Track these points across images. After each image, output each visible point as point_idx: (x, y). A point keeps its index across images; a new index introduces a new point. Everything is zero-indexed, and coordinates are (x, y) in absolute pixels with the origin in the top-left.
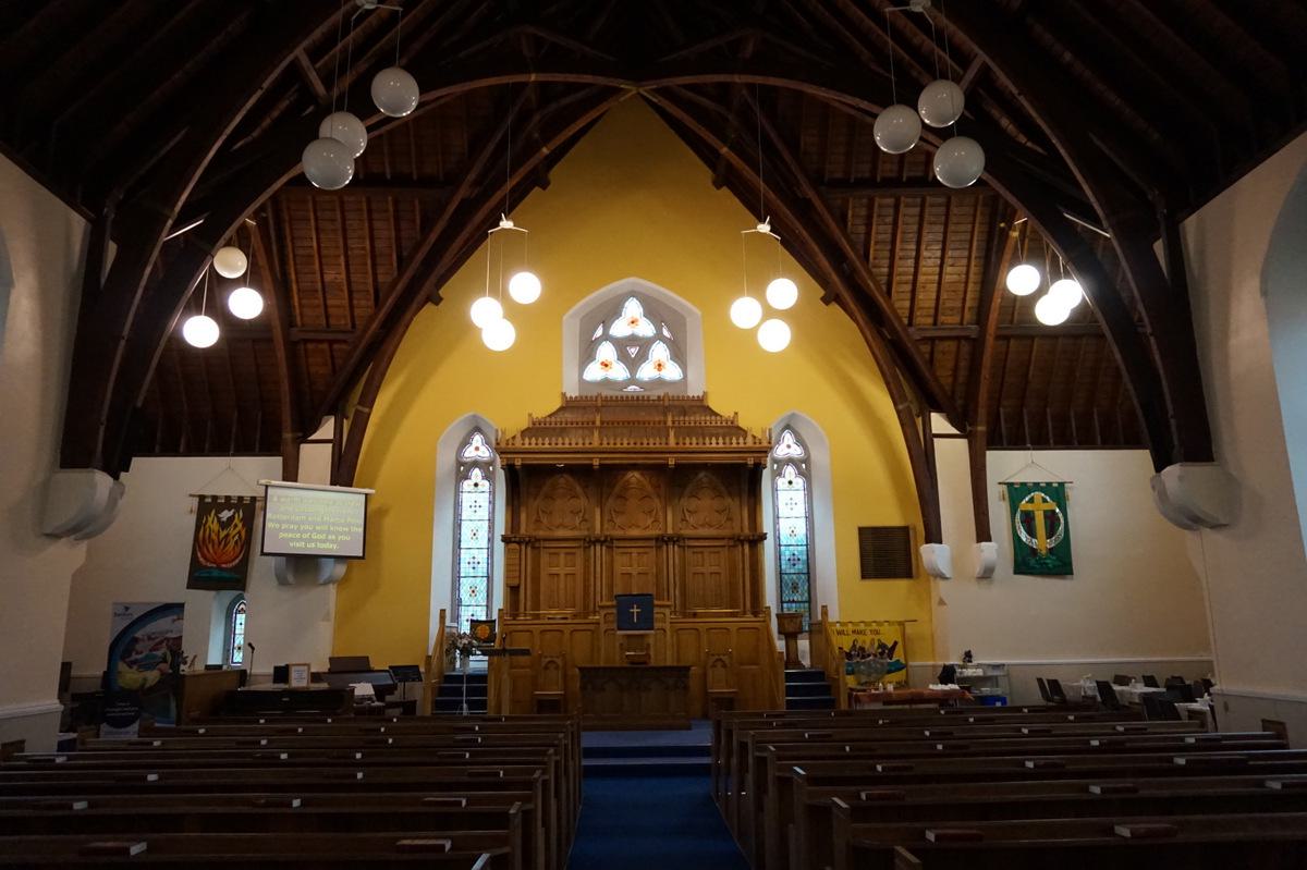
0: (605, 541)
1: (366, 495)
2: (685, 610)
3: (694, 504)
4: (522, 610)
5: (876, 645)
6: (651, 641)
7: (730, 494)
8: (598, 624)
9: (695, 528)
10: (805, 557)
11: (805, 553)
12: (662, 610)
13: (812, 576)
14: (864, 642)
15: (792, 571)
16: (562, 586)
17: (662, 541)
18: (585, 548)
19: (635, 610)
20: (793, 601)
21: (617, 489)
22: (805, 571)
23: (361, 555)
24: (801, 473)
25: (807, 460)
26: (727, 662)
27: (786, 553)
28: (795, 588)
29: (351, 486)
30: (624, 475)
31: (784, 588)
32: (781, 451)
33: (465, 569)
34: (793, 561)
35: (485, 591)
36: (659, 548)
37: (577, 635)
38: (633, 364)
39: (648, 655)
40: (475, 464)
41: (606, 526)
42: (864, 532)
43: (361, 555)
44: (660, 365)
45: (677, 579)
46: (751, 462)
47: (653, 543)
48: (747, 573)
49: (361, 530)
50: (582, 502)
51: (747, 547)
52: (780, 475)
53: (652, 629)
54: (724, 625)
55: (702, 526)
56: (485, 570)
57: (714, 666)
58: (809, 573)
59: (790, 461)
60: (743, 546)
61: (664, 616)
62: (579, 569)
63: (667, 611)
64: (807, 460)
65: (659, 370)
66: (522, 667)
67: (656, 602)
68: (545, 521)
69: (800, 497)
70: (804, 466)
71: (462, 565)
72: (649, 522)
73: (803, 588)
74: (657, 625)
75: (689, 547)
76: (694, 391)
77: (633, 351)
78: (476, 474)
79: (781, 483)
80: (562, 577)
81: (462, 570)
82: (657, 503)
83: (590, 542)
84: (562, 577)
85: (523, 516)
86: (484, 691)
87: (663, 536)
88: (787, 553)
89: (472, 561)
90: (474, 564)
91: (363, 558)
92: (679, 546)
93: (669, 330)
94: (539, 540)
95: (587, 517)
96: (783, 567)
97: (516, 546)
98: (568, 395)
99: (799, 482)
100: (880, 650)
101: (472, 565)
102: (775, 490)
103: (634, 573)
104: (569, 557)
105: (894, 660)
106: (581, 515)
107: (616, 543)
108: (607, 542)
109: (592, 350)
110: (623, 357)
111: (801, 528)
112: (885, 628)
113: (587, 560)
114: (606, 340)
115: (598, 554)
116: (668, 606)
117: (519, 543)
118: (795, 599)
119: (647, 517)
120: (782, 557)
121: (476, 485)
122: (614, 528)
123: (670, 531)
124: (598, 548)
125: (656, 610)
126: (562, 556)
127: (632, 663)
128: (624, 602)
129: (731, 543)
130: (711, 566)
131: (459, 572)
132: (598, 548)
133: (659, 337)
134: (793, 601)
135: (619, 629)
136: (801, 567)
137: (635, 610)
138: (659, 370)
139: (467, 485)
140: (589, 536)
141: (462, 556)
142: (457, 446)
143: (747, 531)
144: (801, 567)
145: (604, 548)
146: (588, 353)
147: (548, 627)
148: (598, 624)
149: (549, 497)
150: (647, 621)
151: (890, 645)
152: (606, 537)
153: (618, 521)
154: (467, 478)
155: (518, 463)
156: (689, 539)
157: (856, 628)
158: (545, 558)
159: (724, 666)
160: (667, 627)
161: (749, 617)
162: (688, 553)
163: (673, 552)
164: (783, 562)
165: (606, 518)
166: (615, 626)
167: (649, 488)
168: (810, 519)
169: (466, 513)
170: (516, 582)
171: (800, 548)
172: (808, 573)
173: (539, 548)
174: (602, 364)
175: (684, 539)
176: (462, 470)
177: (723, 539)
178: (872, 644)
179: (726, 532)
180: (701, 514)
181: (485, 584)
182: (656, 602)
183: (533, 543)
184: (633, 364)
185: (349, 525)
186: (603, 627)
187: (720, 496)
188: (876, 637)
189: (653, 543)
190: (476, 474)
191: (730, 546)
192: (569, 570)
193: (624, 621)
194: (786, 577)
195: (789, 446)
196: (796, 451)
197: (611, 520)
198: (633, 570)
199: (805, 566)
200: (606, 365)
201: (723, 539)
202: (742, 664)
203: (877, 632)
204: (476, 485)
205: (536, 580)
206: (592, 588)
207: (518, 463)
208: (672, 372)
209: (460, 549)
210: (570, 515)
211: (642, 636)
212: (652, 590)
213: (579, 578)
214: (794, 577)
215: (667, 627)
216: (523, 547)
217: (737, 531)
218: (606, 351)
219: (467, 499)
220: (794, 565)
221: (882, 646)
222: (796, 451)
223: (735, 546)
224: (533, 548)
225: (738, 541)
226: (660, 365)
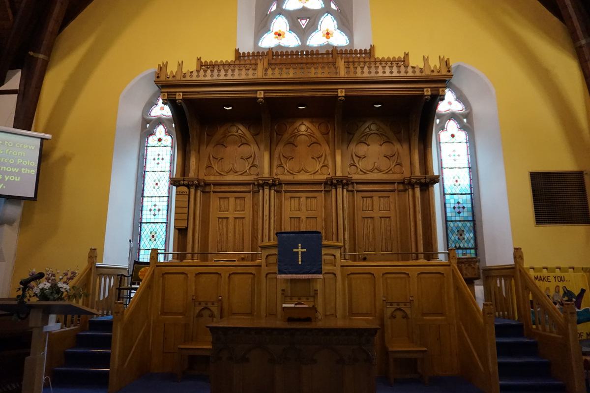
0: (274, 185)
1: (42, 139)
2: (355, 251)
3: (362, 149)
4: (189, 250)
5: (562, 292)
6: (319, 286)
7: (400, 141)
8: (260, 266)
9: (365, 173)
10: (469, 206)
11: (469, 201)
12: (331, 251)
13: (477, 223)
14: (548, 289)
15: (458, 219)
16: (231, 227)
17: (332, 184)
18: (254, 192)
19: (300, 250)
20: (460, 248)
21: (286, 136)
22: (470, 218)
23: (33, 196)
24: (463, 127)
25: (468, 115)
26: (408, 312)
27: (451, 201)
28: (461, 233)
29: (30, 130)
30: (293, 123)
31: (450, 235)
32: (443, 107)
33: (147, 216)
34: (459, 209)
35: (163, 236)
36: (327, 192)
37: (236, 278)
38: (303, 34)
39: (314, 309)
40: (159, 121)
41: (275, 171)
42: (536, 178)
43: (33, 196)
44: (328, 34)
45: (346, 215)
46: (428, 92)
47: (322, 188)
48: (419, 216)
49: (34, 172)
50: (253, 149)
51: (418, 190)
52: (443, 129)
53: (321, 273)
54: (367, 269)
55: (372, 171)
56: (165, 216)
57: (393, 316)
58: (475, 221)
59: (453, 116)
60: (413, 189)
61: (334, 260)
62: (248, 214)
63: (338, 253)
64: (468, 115)
65: (328, 38)
66: (175, 314)
67: (325, 242)
68: (216, 167)
69: (462, 150)
70: (465, 120)
71: (144, 212)
72: (318, 167)
73: (469, 235)
74: (326, 268)
75: (358, 191)
76: (361, 44)
77: (304, 23)
78: (160, 131)
79: (444, 136)
80: (231, 220)
81: (144, 216)
82: (326, 149)
83: (261, 185)
84: (231, 220)
85: (193, 160)
86: (107, 342)
87: (331, 179)
88: (452, 201)
89: (153, 208)
90: (155, 210)
91: (35, 199)
92: (348, 191)
93: (336, 4)
94: (209, 185)
95: (256, 162)
96: (449, 215)
97: (185, 189)
98: (241, 51)
99: (462, 136)
100: (566, 298)
101: (153, 212)
102: (439, 143)
103: (303, 217)
104: (238, 201)
105: (582, 309)
106: (251, 160)
107: (284, 188)
108: (275, 185)
109: (266, 22)
110: (294, 27)
111: (465, 182)
112: (570, 275)
113: (255, 204)
114: (280, 14)
115: (267, 198)
116: (340, 247)
117: (188, 186)
118: (462, 246)
119: (312, 156)
120: (447, 205)
121: (160, 140)
122: (283, 174)
123: (339, 174)
124: (267, 191)
125: (324, 251)
126: (232, 200)
127: (290, 320)
128: (286, 240)
129: (401, 187)
130: (380, 209)
131: (141, 219)
132: (267, 191)
133: (327, 10)
134: (460, 248)
135: (281, 272)
136: (466, 214)
137: (300, 250)
138: (328, 38)
139: (152, 140)
140: (257, 180)
141: (145, 204)
142: (143, 105)
143: (418, 173)
144: (466, 214)
145: (273, 191)
146: (263, 25)
147: (240, 270)
148: (260, 266)
149: (221, 144)
150: (313, 263)
151: (577, 292)
152: (274, 180)
153: (288, 166)
154: (152, 134)
155: (179, 97)
156: (358, 183)
157: (539, 274)
158: (214, 201)
159: (406, 317)
160: (338, 270)
161: (422, 261)
162: (358, 197)
163: (342, 194)
164: (448, 210)
165: (276, 163)
166: (275, 269)
167: (318, 134)
168: (473, 169)
169: (150, 165)
170: (183, 224)
171: (464, 196)
172: (474, 221)
173: (209, 192)
174: (276, 33)
175: (352, 183)
176: (147, 127)
177: (393, 183)
178: (557, 291)
179: (397, 177)
180: (371, 157)
181: (164, 230)
182: (325, 242)
183: (202, 186)
184: (303, 34)
185: (20, 166)
186: (265, 270)
187: (388, 141)
188: (561, 284)
189: (322, 188)
190: (160, 131)
191: (399, 191)
192: (238, 214)
193: (286, 262)
194: (452, 224)
195: (450, 103)
196: (458, 107)
197: (280, 166)
198: (299, 211)
199: (470, 214)
200: (280, 35)
201: (393, 183)
202: (424, 314)
203: (562, 279)
204: (160, 140)
205: (205, 222)
206: (260, 231)
207: (179, 97)
208: (340, 40)
209: (143, 196)
210: (243, 157)
211: (308, 281)
212: (319, 226)
213: (248, 221)
214: (460, 224)
215: (338, 270)
216: (192, 191)
217: (407, 174)
218: (280, 23)
219: (151, 153)
220: (459, 213)
221: (568, 293)
222: (458, 107)
223: (405, 190)
224: (204, 192)
225: (408, 184)
226: (328, 34)
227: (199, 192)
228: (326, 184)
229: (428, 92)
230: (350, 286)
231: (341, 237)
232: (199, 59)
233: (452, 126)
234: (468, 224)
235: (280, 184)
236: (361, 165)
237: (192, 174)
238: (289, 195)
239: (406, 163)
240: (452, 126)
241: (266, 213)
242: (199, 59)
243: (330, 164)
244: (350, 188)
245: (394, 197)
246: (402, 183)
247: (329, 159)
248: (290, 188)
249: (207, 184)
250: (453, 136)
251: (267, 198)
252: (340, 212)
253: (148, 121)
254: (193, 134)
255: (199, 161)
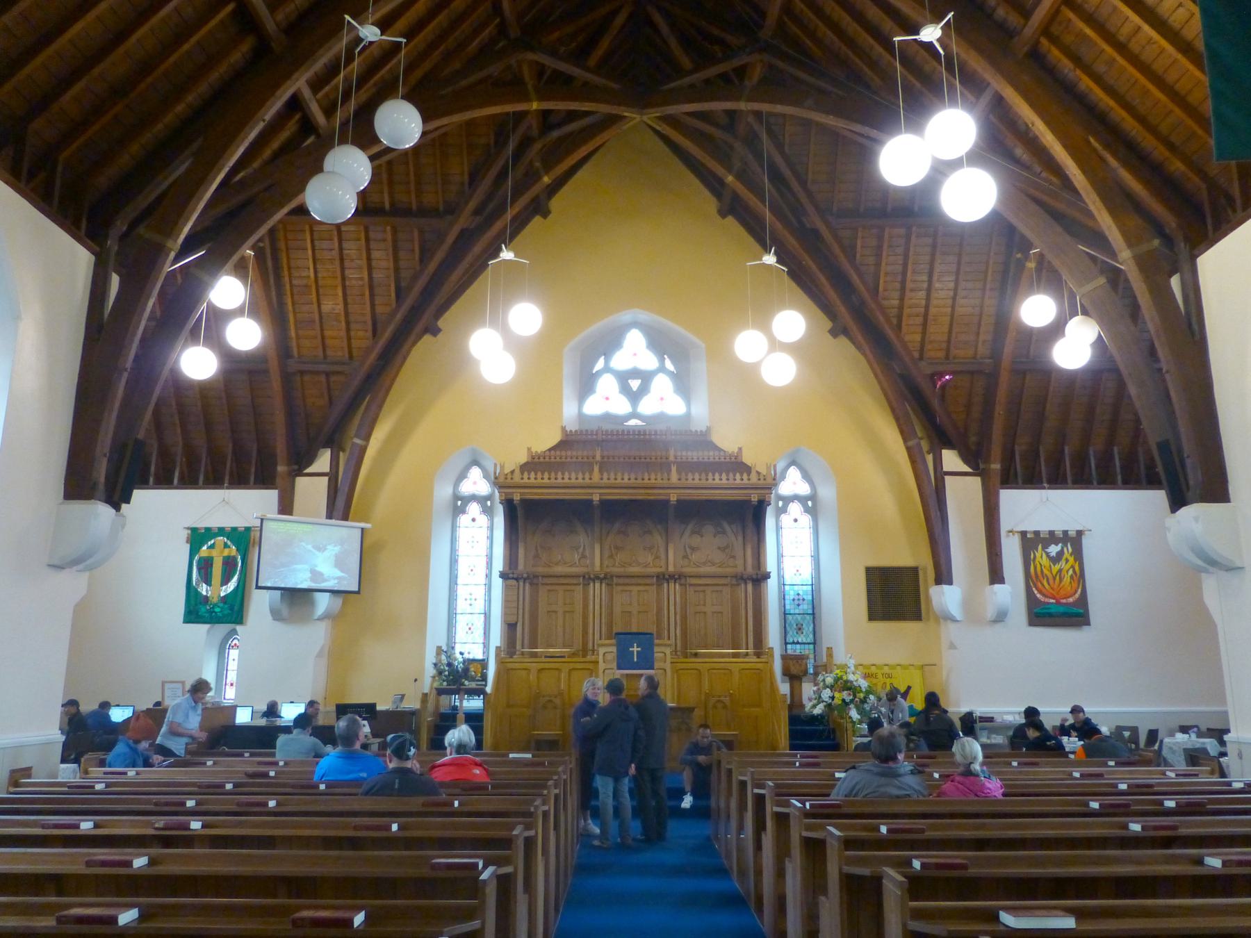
3: (696, 540)
12: (662, 649)
13: (817, 616)
15: (797, 611)
16: (560, 622)
17: (663, 578)
25: (813, 497)
28: (800, 629)
32: (785, 488)
33: (461, 605)
34: (798, 600)
36: (659, 585)
38: (634, 397)
41: (606, 563)
42: (869, 571)
46: (755, 499)
51: (750, 587)
57: (715, 707)
73: (808, 628)
74: (656, 665)
78: (474, 508)
91: (358, 592)
96: (788, 607)
97: (514, 582)
99: (806, 520)
115: (597, 592)
117: (517, 579)
123: (671, 569)
125: (656, 649)
133: (662, 369)
136: (805, 607)
139: (464, 520)
143: (750, 570)
144: (806, 607)
146: (586, 385)
147: (547, 666)
155: (517, 498)
158: (543, 591)
159: (725, 707)
163: (674, 589)
164: (787, 602)
170: (512, 620)
176: (459, 505)
179: (729, 570)
180: (704, 550)
182: (656, 641)
188: (888, 681)
190: (474, 508)
198: (634, 606)
203: (890, 676)
207: (517, 498)
214: (799, 617)
215: (668, 666)
217: (740, 569)
225: (741, 579)
227: (527, 586)
228: (658, 577)
229: (755, 499)
230: (679, 681)
231: (672, 634)
232: (529, 449)
233: (795, 509)
234: (808, 617)
235: (612, 577)
236: (694, 557)
237: (521, 567)
238: (620, 588)
239: (739, 553)
240: (795, 509)
241: (597, 607)
242: (529, 449)
243: (663, 556)
244: (683, 581)
245: (726, 590)
246: (735, 576)
247: (662, 550)
248: (621, 581)
249: (536, 577)
250: (796, 520)
251: (597, 592)
252: (672, 608)
253: (461, 498)
254: (520, 522)
255: (526, 549)
